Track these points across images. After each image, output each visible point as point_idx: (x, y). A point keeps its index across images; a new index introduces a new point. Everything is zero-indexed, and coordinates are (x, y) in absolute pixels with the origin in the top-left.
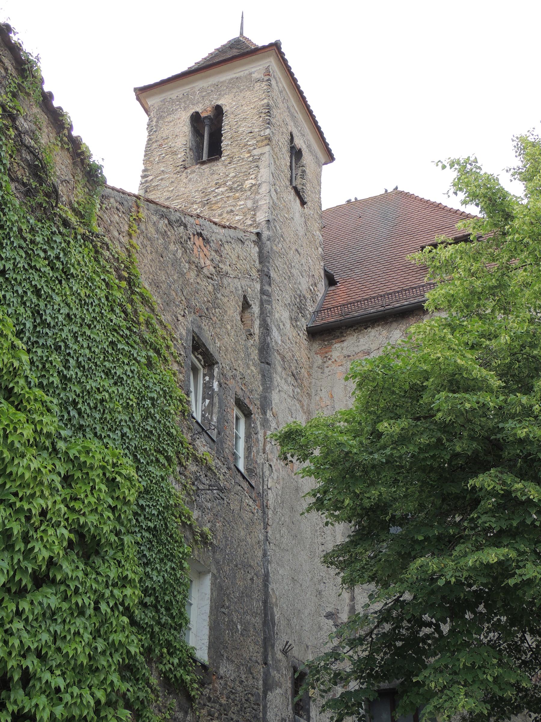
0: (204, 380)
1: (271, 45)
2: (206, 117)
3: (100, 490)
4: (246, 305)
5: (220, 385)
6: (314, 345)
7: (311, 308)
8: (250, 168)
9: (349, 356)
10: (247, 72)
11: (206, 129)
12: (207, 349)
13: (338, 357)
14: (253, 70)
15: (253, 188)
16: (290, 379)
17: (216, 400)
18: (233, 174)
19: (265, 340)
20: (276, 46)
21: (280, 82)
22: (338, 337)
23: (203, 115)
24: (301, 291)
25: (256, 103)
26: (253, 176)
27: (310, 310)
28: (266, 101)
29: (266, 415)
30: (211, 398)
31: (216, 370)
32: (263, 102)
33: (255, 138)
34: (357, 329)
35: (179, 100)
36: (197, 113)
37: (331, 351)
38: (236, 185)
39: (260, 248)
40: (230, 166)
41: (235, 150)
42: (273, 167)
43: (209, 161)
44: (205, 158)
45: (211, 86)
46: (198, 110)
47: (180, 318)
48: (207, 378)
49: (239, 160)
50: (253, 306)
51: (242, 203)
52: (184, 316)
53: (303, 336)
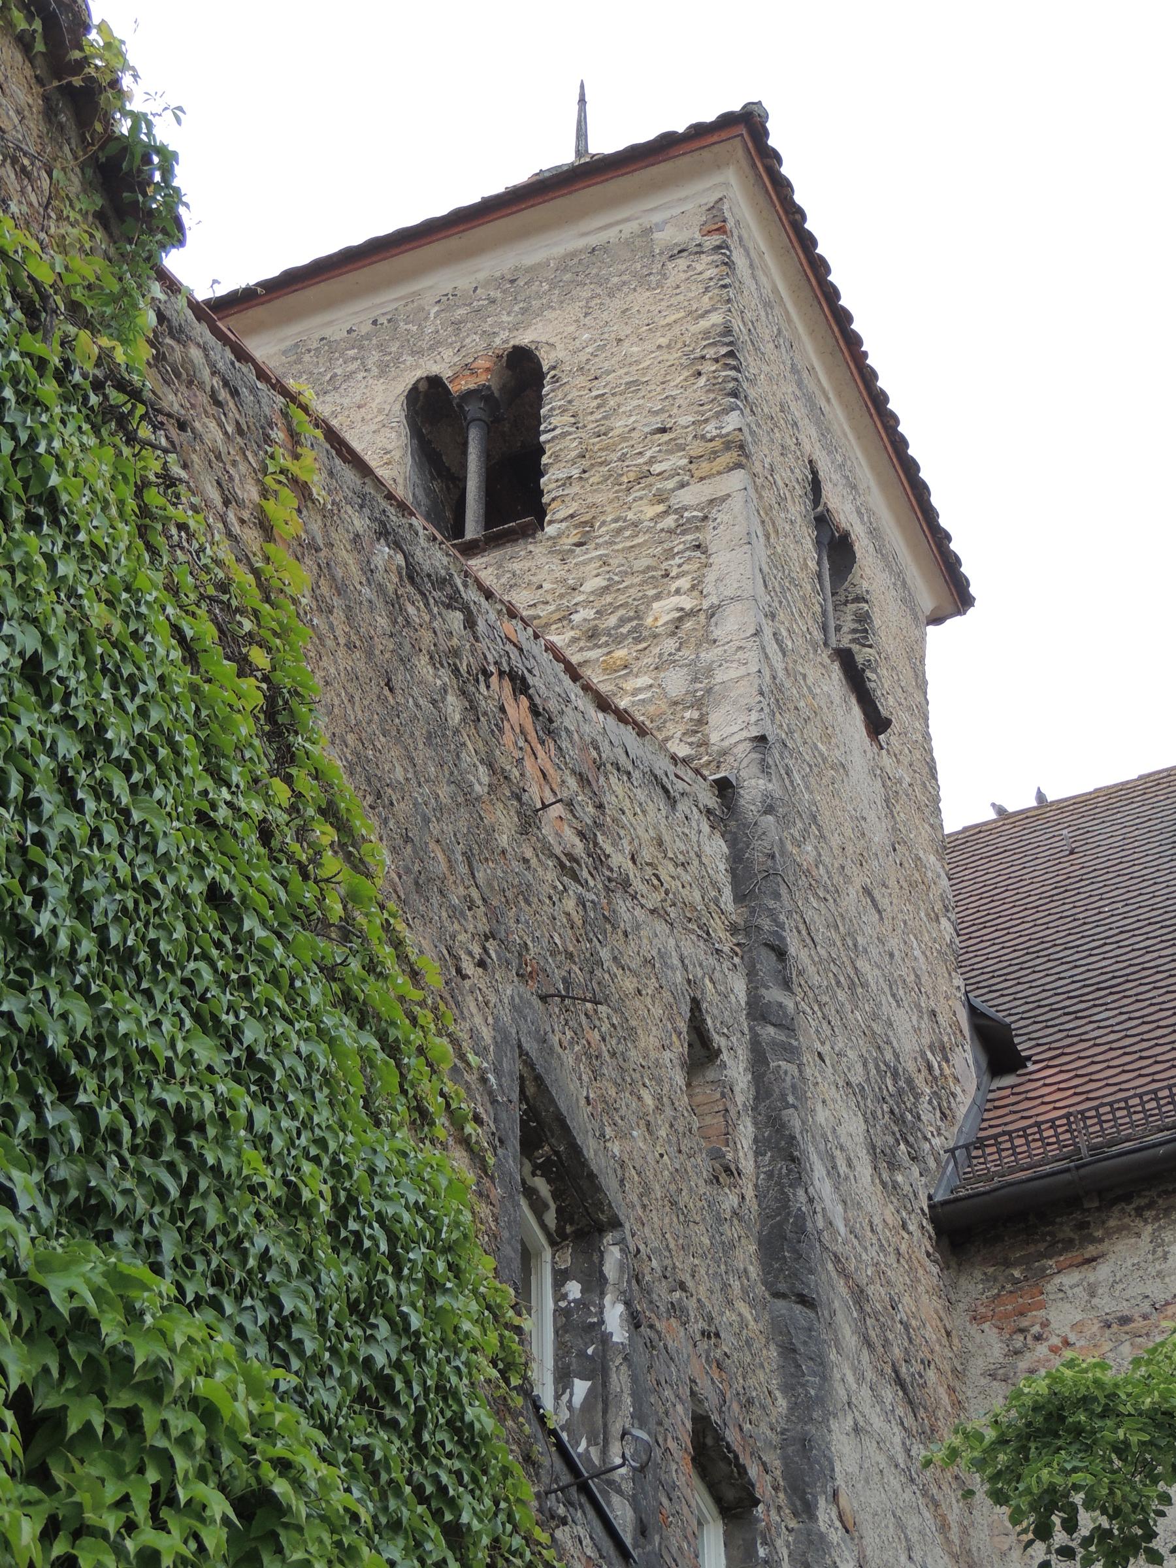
0: (559, 1296)
1: (727, 121)
2: (470, 394)
3: (197, 1509)
4: (702, 1052)
5: (634, 1320)
6: (963, 1282)
7: (939, 1140)
8: (670, 554)
9: (1125, 1320)
10: (633, 227)
11: (474, 439)
12: (575, 1150)
13: (1076, 1326)
14: (657, 218)
15: (688, 625)
16: (889, 1394)
17: (620, 1380)
18: (600, 582)
19: (784, 1203)
20: (746, 127)
21: (764, 269)
22: (1069, 1245)
23: (457, 387)
24: (896, 1056)
25: (676, 330)
26: (684, 583)
27: (936, 1141)
28: (716, 318)
29: (813, 1517)
30: (598, 1371)
31: (613, 1257)
32: (704, 324)
33: (681, 448)
34: (1150, 1206)
35: (354, 339)
36: (435, 382)
37: (1042, 1306)
38: (612, 620)
39: (732, 842)
40: (580, 555)
41: (599, 498)
42: (762, 553)
43: (494, 540)
44: (472, 530)
45: (487, 283)
46: (435, 369)
47: (468, 967)
48: (574, 1289)
49: (619, 531)
50: (725, 1056)
51: (643, 681)
52: (481, 964)
53: (919, 1240)
